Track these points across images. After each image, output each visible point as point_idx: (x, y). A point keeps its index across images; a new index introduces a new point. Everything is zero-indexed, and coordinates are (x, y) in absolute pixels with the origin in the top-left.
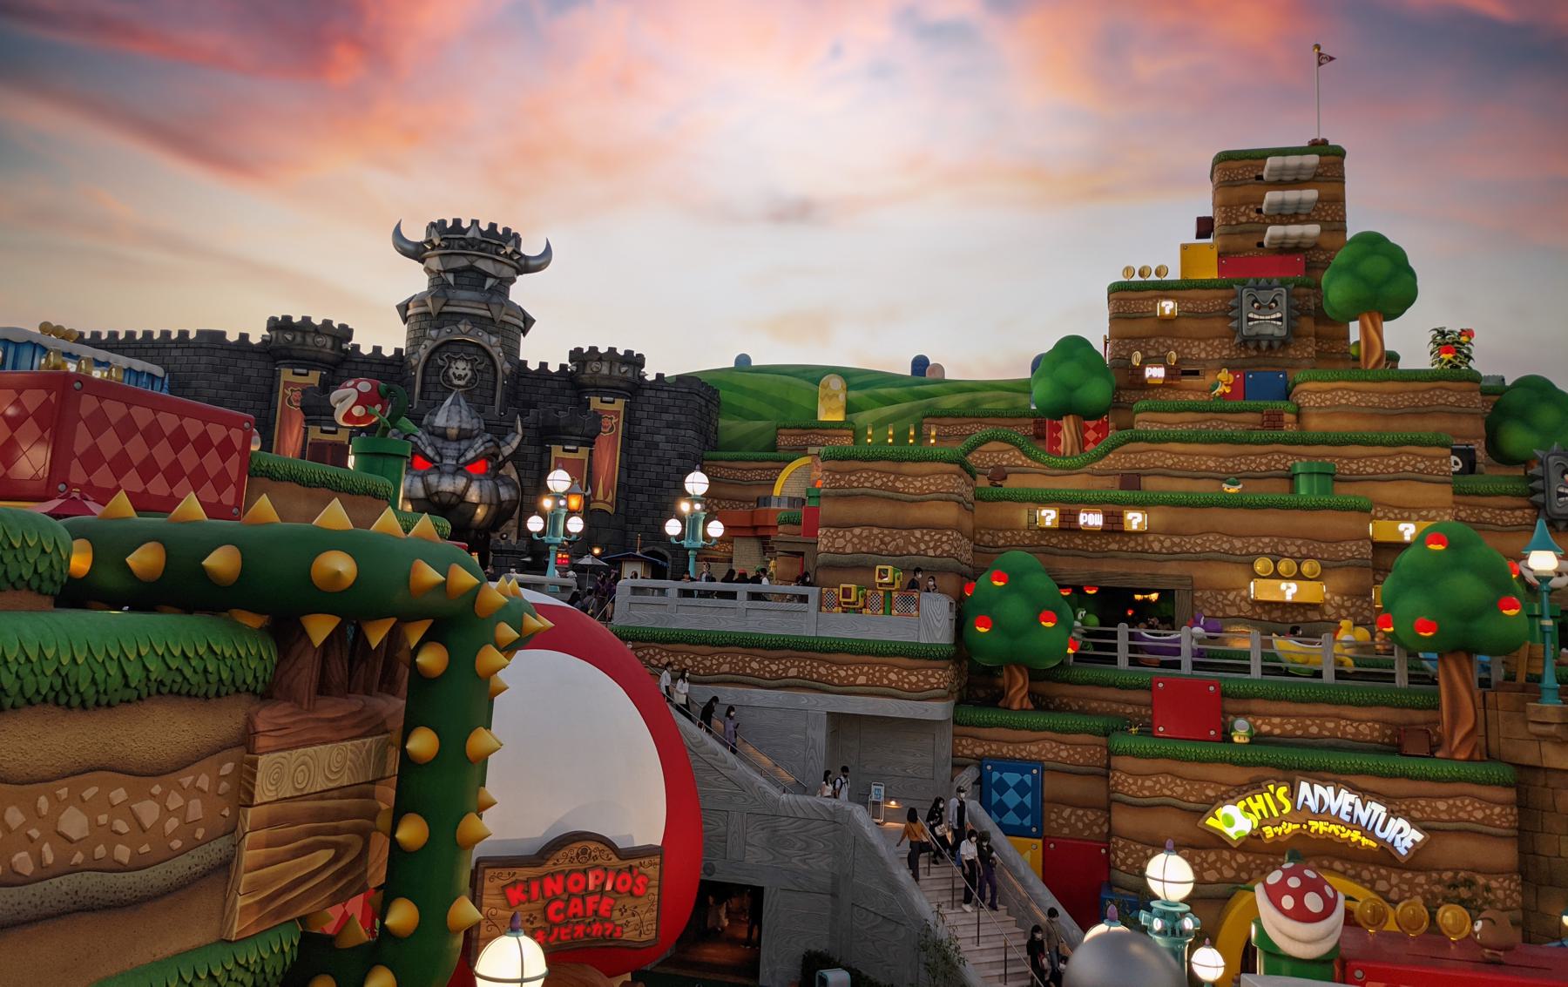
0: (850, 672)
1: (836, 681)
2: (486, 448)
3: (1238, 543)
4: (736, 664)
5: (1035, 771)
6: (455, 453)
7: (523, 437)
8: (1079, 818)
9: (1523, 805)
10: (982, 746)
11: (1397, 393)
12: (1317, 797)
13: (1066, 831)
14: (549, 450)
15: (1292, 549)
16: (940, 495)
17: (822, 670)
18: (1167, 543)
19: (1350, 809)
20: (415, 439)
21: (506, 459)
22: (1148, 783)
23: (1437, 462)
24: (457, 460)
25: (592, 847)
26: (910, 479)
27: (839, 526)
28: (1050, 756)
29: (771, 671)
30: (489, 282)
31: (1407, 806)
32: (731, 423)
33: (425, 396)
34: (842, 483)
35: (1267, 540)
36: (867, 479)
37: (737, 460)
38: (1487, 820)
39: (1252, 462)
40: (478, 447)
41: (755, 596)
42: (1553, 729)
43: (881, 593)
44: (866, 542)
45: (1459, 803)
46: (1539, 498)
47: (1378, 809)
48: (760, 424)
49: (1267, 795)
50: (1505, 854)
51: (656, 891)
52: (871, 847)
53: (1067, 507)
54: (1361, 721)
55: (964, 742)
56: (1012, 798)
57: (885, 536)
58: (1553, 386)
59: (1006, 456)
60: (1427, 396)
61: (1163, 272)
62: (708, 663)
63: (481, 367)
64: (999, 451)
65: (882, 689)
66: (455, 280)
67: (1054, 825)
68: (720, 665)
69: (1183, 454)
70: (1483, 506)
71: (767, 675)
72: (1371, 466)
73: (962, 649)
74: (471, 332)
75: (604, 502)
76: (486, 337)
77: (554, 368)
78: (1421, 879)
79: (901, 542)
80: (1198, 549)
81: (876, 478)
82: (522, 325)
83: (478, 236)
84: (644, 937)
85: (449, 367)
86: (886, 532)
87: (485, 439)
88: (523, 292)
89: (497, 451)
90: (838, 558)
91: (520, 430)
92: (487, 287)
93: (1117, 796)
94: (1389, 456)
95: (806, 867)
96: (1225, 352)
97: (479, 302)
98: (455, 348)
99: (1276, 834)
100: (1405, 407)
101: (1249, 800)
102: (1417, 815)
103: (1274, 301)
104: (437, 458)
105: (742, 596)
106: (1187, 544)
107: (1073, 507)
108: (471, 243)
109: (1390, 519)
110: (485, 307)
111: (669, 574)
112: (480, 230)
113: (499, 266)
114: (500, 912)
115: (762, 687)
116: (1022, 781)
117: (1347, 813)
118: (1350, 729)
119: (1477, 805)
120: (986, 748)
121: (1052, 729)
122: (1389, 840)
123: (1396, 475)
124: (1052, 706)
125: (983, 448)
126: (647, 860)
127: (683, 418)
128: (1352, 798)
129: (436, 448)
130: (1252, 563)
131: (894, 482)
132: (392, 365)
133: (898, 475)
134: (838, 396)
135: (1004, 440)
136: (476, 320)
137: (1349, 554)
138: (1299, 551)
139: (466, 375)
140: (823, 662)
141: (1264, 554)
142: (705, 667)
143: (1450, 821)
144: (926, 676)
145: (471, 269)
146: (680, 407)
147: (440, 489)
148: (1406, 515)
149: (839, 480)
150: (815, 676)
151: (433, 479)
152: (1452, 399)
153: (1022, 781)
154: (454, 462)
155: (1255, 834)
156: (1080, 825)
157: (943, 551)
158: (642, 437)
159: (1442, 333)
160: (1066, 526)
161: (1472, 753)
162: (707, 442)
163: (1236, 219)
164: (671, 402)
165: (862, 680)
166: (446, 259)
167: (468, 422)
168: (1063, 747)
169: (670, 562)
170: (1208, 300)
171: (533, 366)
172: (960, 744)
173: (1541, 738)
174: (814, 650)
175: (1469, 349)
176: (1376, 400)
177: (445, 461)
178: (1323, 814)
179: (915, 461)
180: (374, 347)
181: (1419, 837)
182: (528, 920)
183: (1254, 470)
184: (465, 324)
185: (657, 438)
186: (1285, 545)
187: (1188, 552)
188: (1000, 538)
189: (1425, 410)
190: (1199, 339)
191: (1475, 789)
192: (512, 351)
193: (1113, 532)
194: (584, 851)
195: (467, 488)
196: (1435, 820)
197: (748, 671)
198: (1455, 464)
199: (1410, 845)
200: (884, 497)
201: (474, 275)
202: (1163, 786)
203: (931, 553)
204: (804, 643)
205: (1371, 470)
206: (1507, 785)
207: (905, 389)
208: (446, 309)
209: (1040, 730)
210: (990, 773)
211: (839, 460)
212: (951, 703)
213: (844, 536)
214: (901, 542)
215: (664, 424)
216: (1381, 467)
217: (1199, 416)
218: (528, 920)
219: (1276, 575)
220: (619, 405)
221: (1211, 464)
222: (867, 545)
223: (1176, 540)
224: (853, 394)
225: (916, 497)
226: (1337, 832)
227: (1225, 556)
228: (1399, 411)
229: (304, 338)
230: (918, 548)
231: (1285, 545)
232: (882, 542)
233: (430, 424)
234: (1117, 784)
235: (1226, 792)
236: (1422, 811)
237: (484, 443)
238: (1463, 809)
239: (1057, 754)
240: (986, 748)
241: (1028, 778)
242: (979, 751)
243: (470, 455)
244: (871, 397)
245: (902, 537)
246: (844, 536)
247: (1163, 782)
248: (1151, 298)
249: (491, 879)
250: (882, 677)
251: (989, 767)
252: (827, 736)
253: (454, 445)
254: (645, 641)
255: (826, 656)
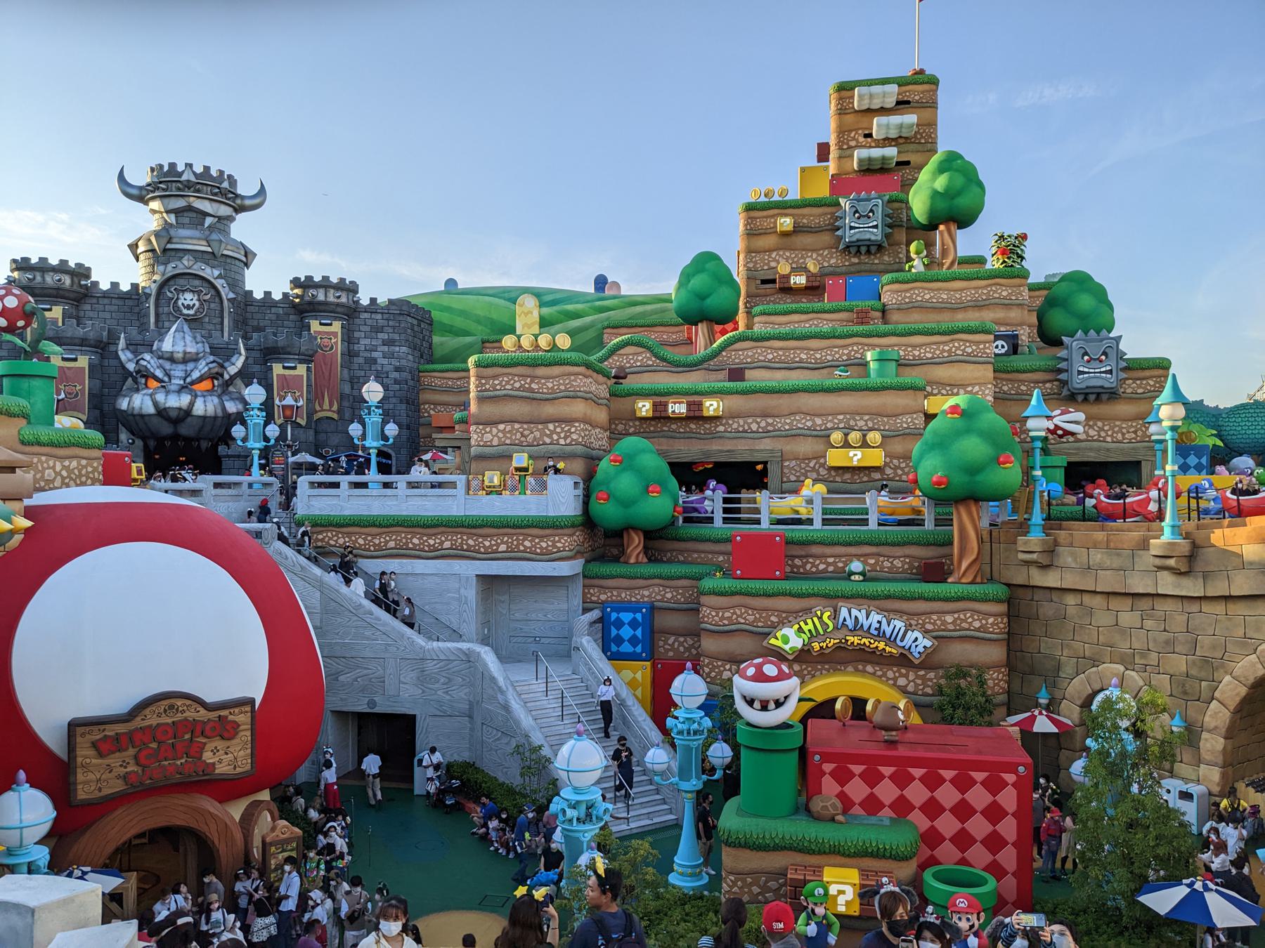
0: (493, 542)
1: (482, 550)
2: (210, 369)
3: (818, 421)
4: (401, 541)
5: (644, 610)
6: (182, 374)
7: (247, 358)
8: (681, 644)
9: (1013, 615)
10: (605, 593)
11: (962, 290)
12: (853, 617)
13: (671, 654)
14: (271, 369)
15: (861, 423)
16: (568, 393)
17: (471, 542)
18: (763, 424)
19: (878, 625)
20: (145, 363)
21: (232, 378)
22: (727, 615)
23: (981, 346)
24: (185, 380)
25: (179, 704)
26: (543, 381)
27: (486, 424)
28: (659, 597)
29: (429, 545)
30: (209, 221)
31: (923, 621)
32: (444, 339)
33: (160, 324)
34: (487, 386)
35: (841, 417)
36: (507, 383)
37: (447, 371)
38: (982, 629)
39: (836, 352)
40: (202, 368)
41: (411, 485)
42: (1035, 556)
43: (517, 478)
44: (508, 435)
45: (962, 617)
46: (1063, 376)
47: (899, 624)
48: (468, 339)
49: (815, 619)
50: (996, 653)
51: (249, 733)
52: (493, 679)
53: (658, 399)
54: (895, 558)
55: (591, 591)
56: (626, 632)
57: (525, 430)
58: (1090, 278)
59: (640, 358)
60: (985, 291)
61: (770, 195)
62: (377, 542)
63: (207, 297)
64: (634, 354)
65: (520, 554)
66: (177, 220)
67: (662, 650)
68: (387, 542)
69: (781, 349)
70: (1020, 381)
71: (426, 548)
72: (930, 352)
73: (588, 522)
74: (195, 267)
75: (330, 410)
76: (208, 270)
77: (277, 296)
78: (932, 675)
79: (538, 434)
80: (787, 427)
81: (515, 382)
82: (244, 259)
83: (193, 179)
84: (239, 770)
85: (178, 299)
86: (525, 426)
87: (208, 361)
88: (243, 229)
89: (220, 370)
90: (487, 450)
91: (243, 351)
92: (206, 225)
93: (703, 626)
94: (944, 343)
95: (448, 697)
96: (833, 261)
97: (199, 239)
98: (181, 281)
99: (821, 648)
100: (968, 301)
101: (802, 624)
102: (929, 627)
103: (871, 211)
104: (166, 379)
105: (344, 486)
106: (779, 423)
107: (663, 399)
108: (188, 185)
109: (943, 395)
110: (205, 243)
111: (394, 469)
112: (194, 173)
113: (215, 205)
114: (93, 761)
115: (423, 558)
116: (634, 619)
117: (876, 629)
118: (887, 564)
119: (976, 617)
120: (609, 594)
121: (660, 577)
122: (907, 647)
123: (950, 359)
124: (665, 559)
125: (622, 351)
126: (237, 710)
127: (396, 337)
128: (879, 617)
129: (165, 370)
130: (829, 436)
131: (530, 384)
132: (130, 299)
133: (533, 377)
134: (532, 313)
135: (639, 344)
136: (198, 256)
137: (905, 425)
138: (866, 425)
139: (194, 305)
140: (470, 535)
141: (838, 428)
142: (375, 545)
143: (954, 630)
144: (554, 542)
145: (190, 208)
146: (394, 327)
147: (167, 405)
148: (955, 391)
149: (485, 384)
150: (465, 547)
151: (160, 397)
152: (1004, 294)
153: (634, 619)
154: (182, 382)
155: (806, 648)
156: (682, 649)
157: (573, 440)
158: (361, 354)
159: (14, 261)
160: (658, 414)
161: (975, 577)
162: (422, 357)
163: (848, 144)
164: (385, 323)
165: (503, 548)
166: (166, 200)
167: (192, 347)
168: (668, 590)
169: (394, 459)
170: (820, 215)
171: (258, 295)
172: (589, 593)
173: (1028, 563)
174: (463, 526)
175: (1022, 250)
176: (945, 297)
177: (173, 381)
178: (857, 628)
179: (546, 365)
180: (112, 283)
181: (928, 643)
182: (121, 766)
183: (837, 360)
184: (188, 260)
185: (375, 355)
186: (856, 420)
187: (779, 430)
188: (631, 427)
189: (983, 303)
190: (813, 250)
191: (977, 606)
192: (235, 283)
193: (659, 418)
194: (171, 707)
195: (192, 404)
196: (943, 630)
197: (411, 546)
198: (1001, 347)
199: (922, 650)
200: (522, 397)
201: (194, 215)
202: (738, 616)
203: (562, 442)
204: (455, 521)
205: (929, 355)
206: (1000, 601)
207: (589, 304)
208: (169, 246)
209: (650, 578)
210: (610, 614)
211: (484, 367)
212: (582, 561)
213: (490, 432)
214: (538, 434)
215: (380, 342)
216: (938, 352)
217: (804, 317)
218: (121, 766)
219: (847, 445)
220: (337, 326)
221: (803, 356)
222: (510, 438)
223: (770, 420)
224: (546, 311)
225: (549, 396)
226: (868, 644)
227: (808, 432)
228: (963, 305)
229: (43, 277)
230: (552, 438)
231: (856, 420)
232: (523, 435)
233: (159, 349)
234: (703, 618)
235: (786, 618)
236: (934, 624)
237: (207, 364)
238: (965, 621)
239: (664, 596)
240: (609, 594)
241: (639, 616)
242: (603, 597)
243: (196, 375)
244: (559, 312)
245: (538, 430)
246: (490, 432)
247: (739, 613)
248: (772, 216)
249: (83, 735)
250: (518, 545)
251: (609, 610)
252: (477, 593)
253: (181, 367)
254: (323, 526)
255: (474, 531)
